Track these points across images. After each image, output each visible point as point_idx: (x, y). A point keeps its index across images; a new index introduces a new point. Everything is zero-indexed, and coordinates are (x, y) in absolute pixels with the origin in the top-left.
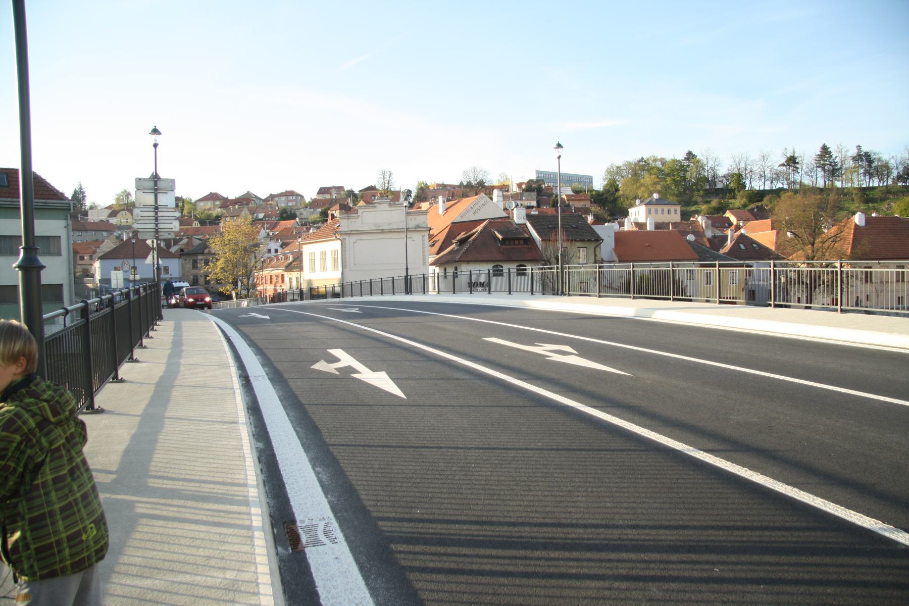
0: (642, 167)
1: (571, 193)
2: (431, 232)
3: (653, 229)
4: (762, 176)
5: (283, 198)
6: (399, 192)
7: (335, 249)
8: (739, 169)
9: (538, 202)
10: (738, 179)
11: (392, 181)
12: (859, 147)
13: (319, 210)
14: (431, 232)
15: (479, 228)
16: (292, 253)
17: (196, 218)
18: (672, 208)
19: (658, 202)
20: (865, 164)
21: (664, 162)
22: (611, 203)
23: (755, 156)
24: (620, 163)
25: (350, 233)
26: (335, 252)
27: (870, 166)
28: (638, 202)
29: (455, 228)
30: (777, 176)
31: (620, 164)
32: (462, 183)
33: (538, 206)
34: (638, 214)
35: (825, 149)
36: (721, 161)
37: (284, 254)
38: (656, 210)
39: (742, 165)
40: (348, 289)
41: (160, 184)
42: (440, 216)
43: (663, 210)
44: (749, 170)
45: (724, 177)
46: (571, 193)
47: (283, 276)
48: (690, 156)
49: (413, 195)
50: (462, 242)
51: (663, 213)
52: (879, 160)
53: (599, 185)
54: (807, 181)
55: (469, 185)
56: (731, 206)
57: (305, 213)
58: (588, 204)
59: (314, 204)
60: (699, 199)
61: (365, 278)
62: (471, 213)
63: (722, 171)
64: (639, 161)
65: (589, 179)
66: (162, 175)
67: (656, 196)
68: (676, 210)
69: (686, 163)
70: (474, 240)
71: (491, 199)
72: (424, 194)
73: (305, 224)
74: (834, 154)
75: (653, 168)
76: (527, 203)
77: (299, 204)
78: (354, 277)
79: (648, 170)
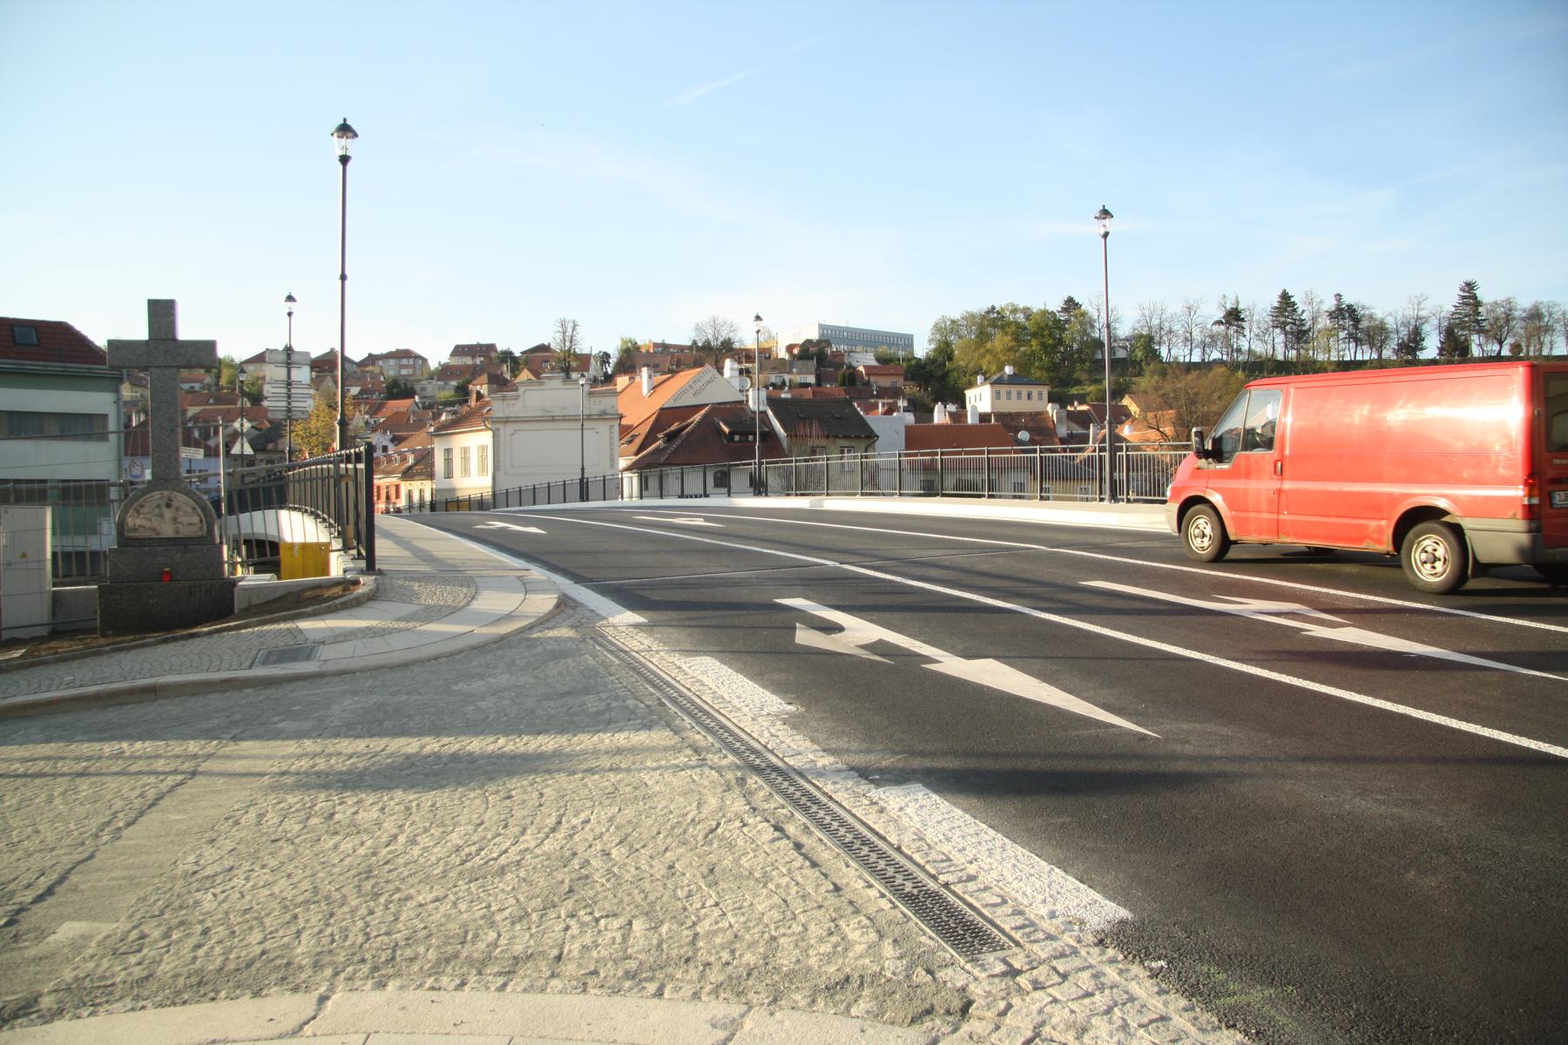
0: (992, 322)
1: (874, 363)
2: (624, 422)
3: (977, 422)
4: (1188, 340)
5: (392, 362)
6: (588, 357)
7: (483, 443)
8: (1150, 328)
9: (818, 378)
10: (1147, 343)
11: (577, 338)
12: (1338, 296)
13: (454, 383)
14: (624, 422)
15: (698, 417)
16: (413, 451)
17: (244, 394)
18: (1035, 390)
19: (1013, 380)
20: (1348, 323)
21: (1027, 313)
22: (936, 378)
23: (1175, 308)
24: (956, 314)
25: (506, 421)
26: (483, 448)
27: (1356, 327)
28: (980, 378)
29: (666, 415)
30: (1211, 341)
31: (957, 316)
32: (695, 342)
33: (819, 383)
34: (980, 399)
35: (1285, 297)
36: (1123, 312)
37: (400, 453)
38: (1009, 393)
39: (1155, 322)
40: (502, 499)
41: (294, 358)
42: (642, 398)
43: (1019, 393)
44: (1166, 329)
45: (1127, 339)
46: (874, 363)
47: (397, 487)
48: (1071, 304)
49: (613, 361)
50: (671, 437)
51: (1040, 398)
52: (1371, 317)
53: (922, 349)
54: (1259, 348)
55: (707, 347)
56: (1134, 387)
57: (429, 388)
58: (900, 382)
59: (445, 372)
60: (1084, 376)
61: (527, 483)
62: (690, 394)
63: (1124, 330)
64: (988, 312)
65: (908, 341)
66: (297, 347)
67: (1008, 370)
68: (1040, 394)
69: (1063, 317)
70: (689, 434)
71: (722, 374)
72: (630, 360)
73: (430, 407)
74: (1300, 307)
75: (1009, 324)
76: (798, 379)
77: (418, 373)
78: (510, 483)
79: (1002, 327)
